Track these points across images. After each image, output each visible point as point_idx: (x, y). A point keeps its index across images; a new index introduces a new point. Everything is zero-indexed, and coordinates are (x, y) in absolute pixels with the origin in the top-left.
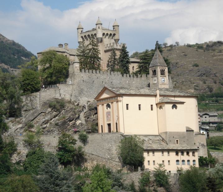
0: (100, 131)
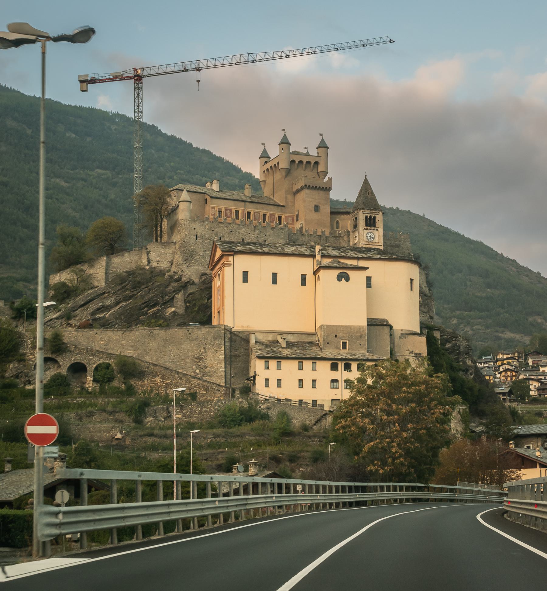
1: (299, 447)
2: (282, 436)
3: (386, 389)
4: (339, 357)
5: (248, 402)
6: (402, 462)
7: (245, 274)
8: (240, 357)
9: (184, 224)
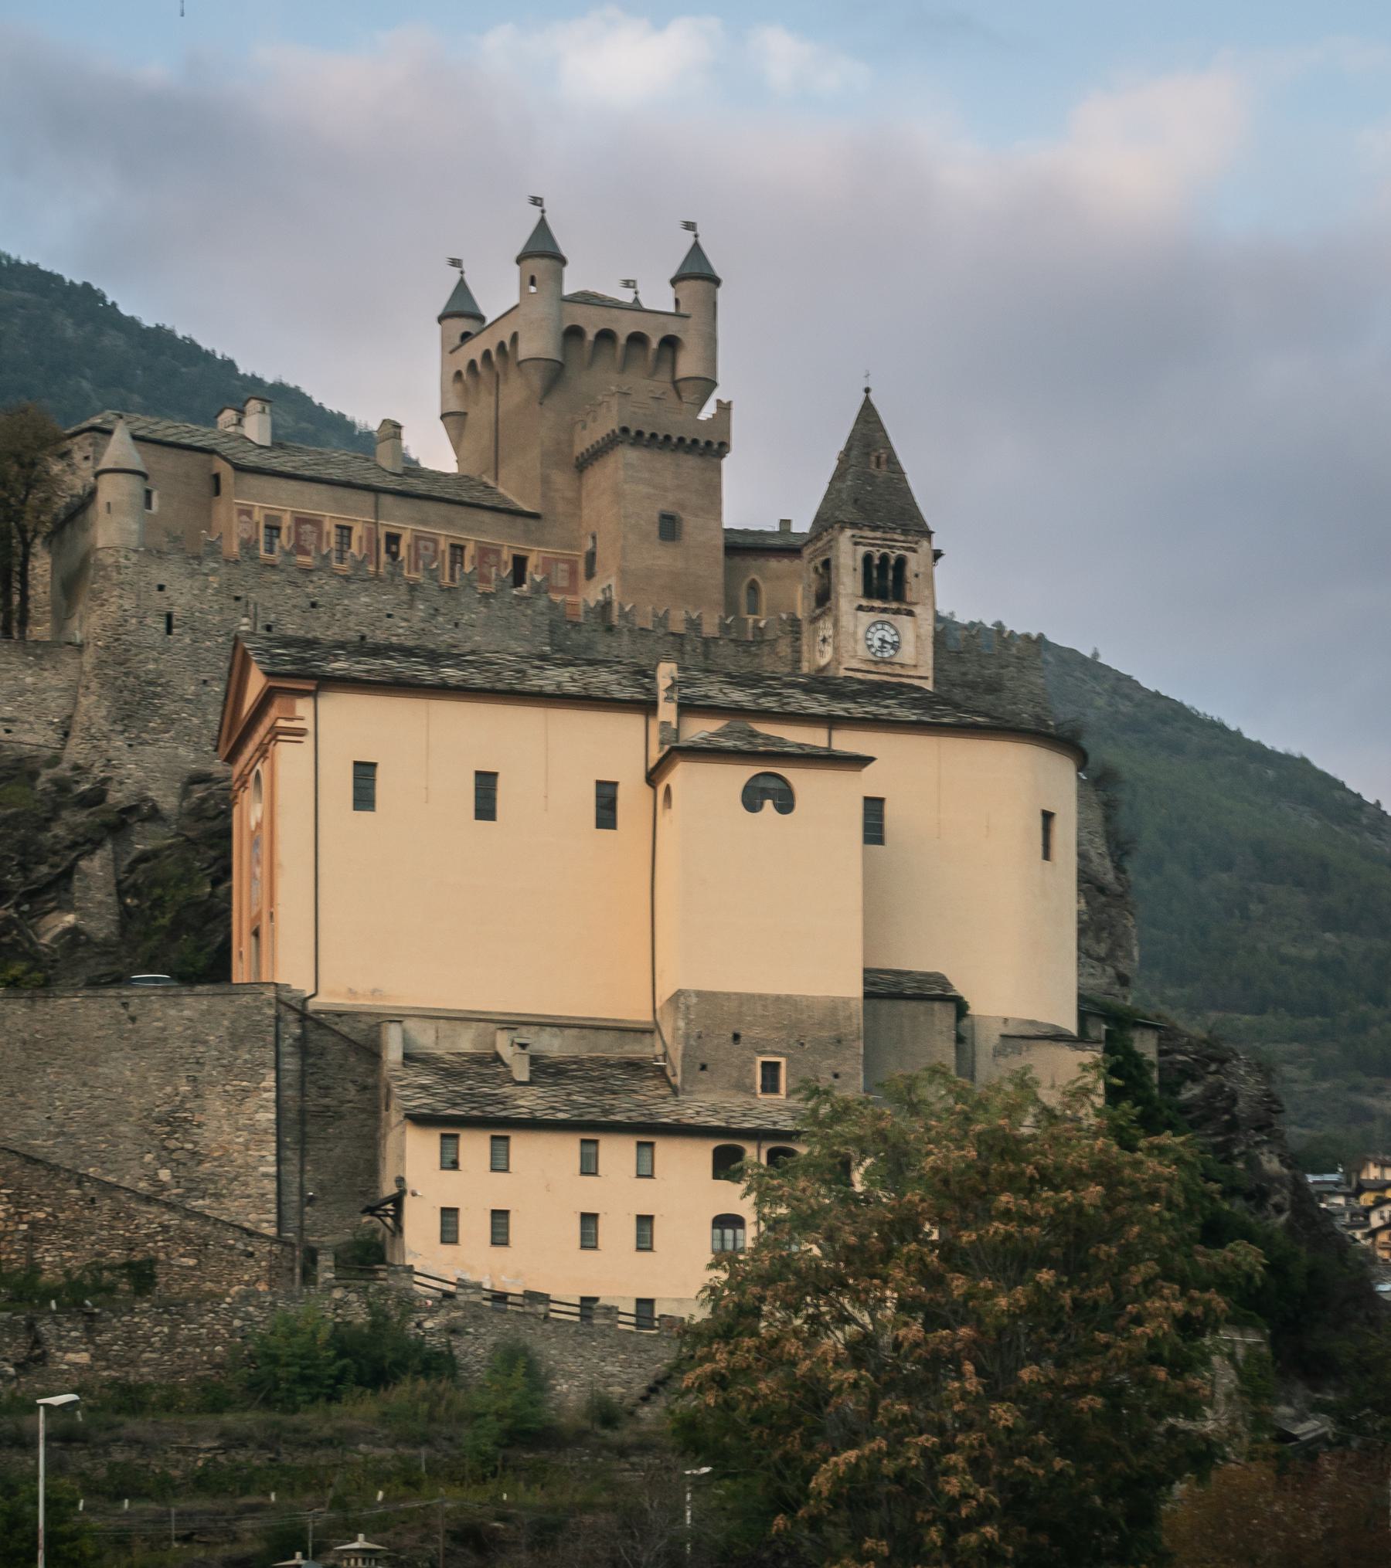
1: (575, 1490)
2: (507, 1446)
3: (922, 1200)
4: (747, 1125)
5: (369, 1305)
6: (990, 1542)
7: (364, 774)
8: (342, 1117)
9: (118, 568)
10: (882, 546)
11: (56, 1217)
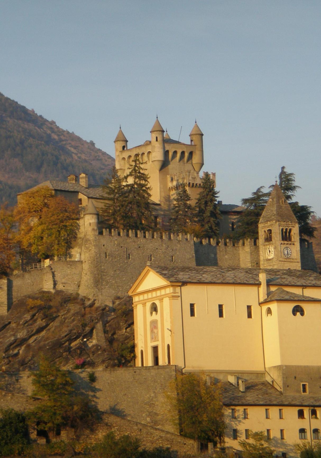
0: (138, 363)
10: (286, 226)
11: (131, 435)
